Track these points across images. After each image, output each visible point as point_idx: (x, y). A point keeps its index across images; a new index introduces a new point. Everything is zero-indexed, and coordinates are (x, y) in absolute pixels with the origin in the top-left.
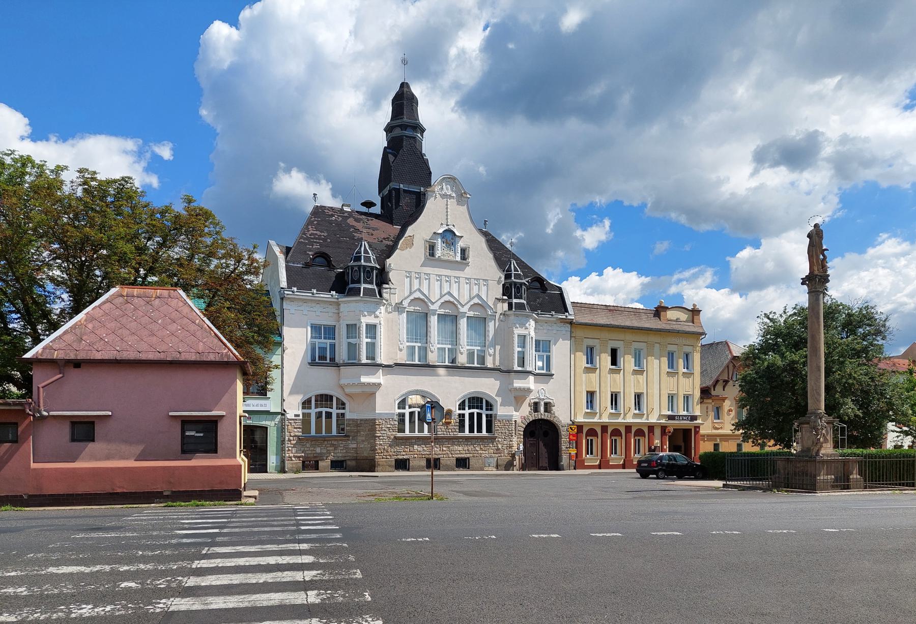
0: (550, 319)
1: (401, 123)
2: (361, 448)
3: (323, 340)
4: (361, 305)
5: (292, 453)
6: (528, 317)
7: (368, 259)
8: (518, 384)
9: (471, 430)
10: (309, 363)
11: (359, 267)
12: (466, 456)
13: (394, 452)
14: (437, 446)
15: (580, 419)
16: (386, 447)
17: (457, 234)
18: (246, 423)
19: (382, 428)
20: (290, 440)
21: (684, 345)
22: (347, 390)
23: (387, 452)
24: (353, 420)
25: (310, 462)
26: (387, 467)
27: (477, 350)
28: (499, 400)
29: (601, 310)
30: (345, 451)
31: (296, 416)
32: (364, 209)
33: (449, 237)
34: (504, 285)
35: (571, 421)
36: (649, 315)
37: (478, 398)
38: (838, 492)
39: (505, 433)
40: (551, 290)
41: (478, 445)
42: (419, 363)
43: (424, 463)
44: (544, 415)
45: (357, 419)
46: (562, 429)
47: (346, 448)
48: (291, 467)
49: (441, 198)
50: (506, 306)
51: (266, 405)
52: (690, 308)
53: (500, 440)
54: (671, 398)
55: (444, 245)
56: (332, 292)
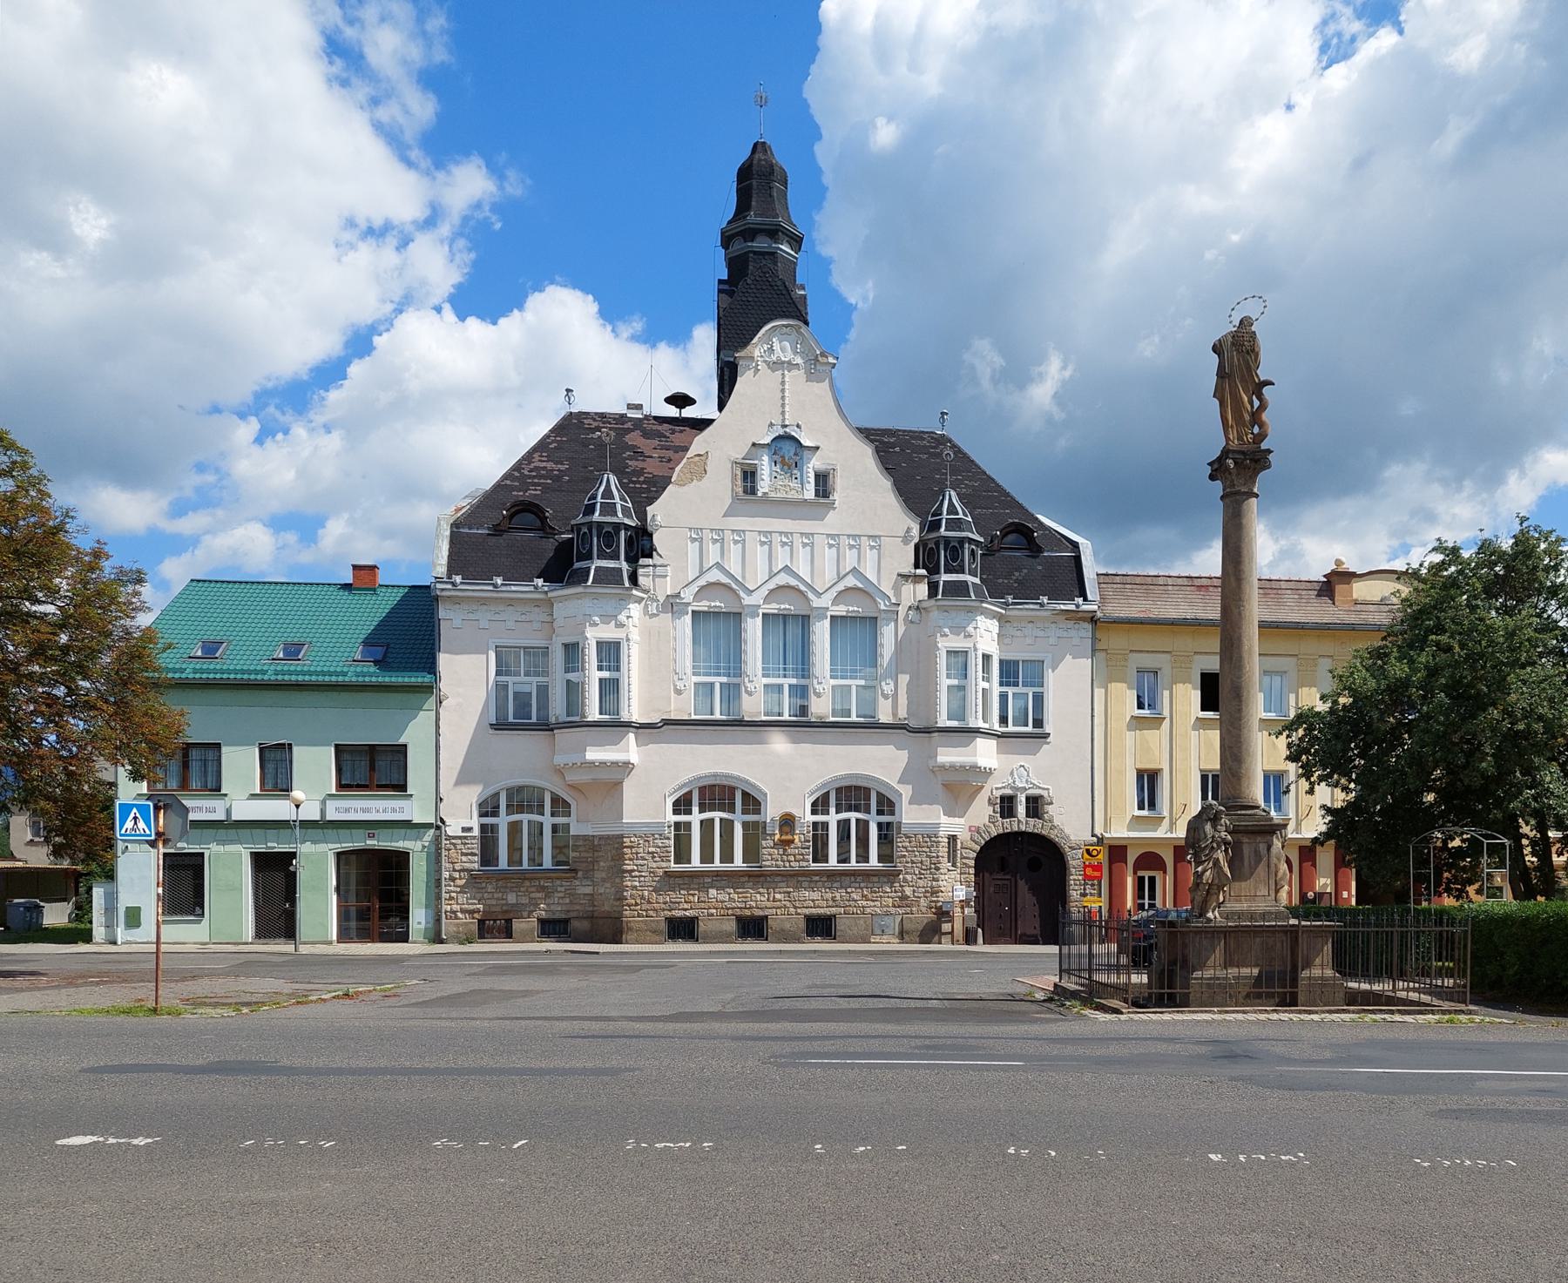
0: (1038, 613)
1: (742, 228)
2: (601, 894)
3: (522, 678)
4: (586, 605)
5: (457, 904)
6: (973, 612)
7: (609, 509)
8: (948, 756)
10: (491, 725)
11: (590, 525)
12: (828, 911)
13: (665, 903)
14: (761, 890)
15: (1119, 831)
16: (646, 893)
17: (806, 442)
18: (366, 845)
20: (453, 879)
22: (572, 778)
23: (649, 902)
24: (585, 838)
25: (495, 921)
27: (721, 684)
28: (906, 791)
29: (1176, 588)
30: (567, 901)
31: (464, 829)
32: (672, 411)
33: (787, 448)
36: (1304, 592)
37: (858, 788)
38: (1202, 1012)
39: (921, 862)
40: (1052, 551)
41: (856, 888)
42: (724, 718)
43: (731, 926)
44: (1027, 823)
46: (1069, 854)
47: (571, 894)
48: (455, 932)
49: (769, 371)
50: (923, 590)
51: (402, 810)
55: (778, 468)
56: (1076, 599)
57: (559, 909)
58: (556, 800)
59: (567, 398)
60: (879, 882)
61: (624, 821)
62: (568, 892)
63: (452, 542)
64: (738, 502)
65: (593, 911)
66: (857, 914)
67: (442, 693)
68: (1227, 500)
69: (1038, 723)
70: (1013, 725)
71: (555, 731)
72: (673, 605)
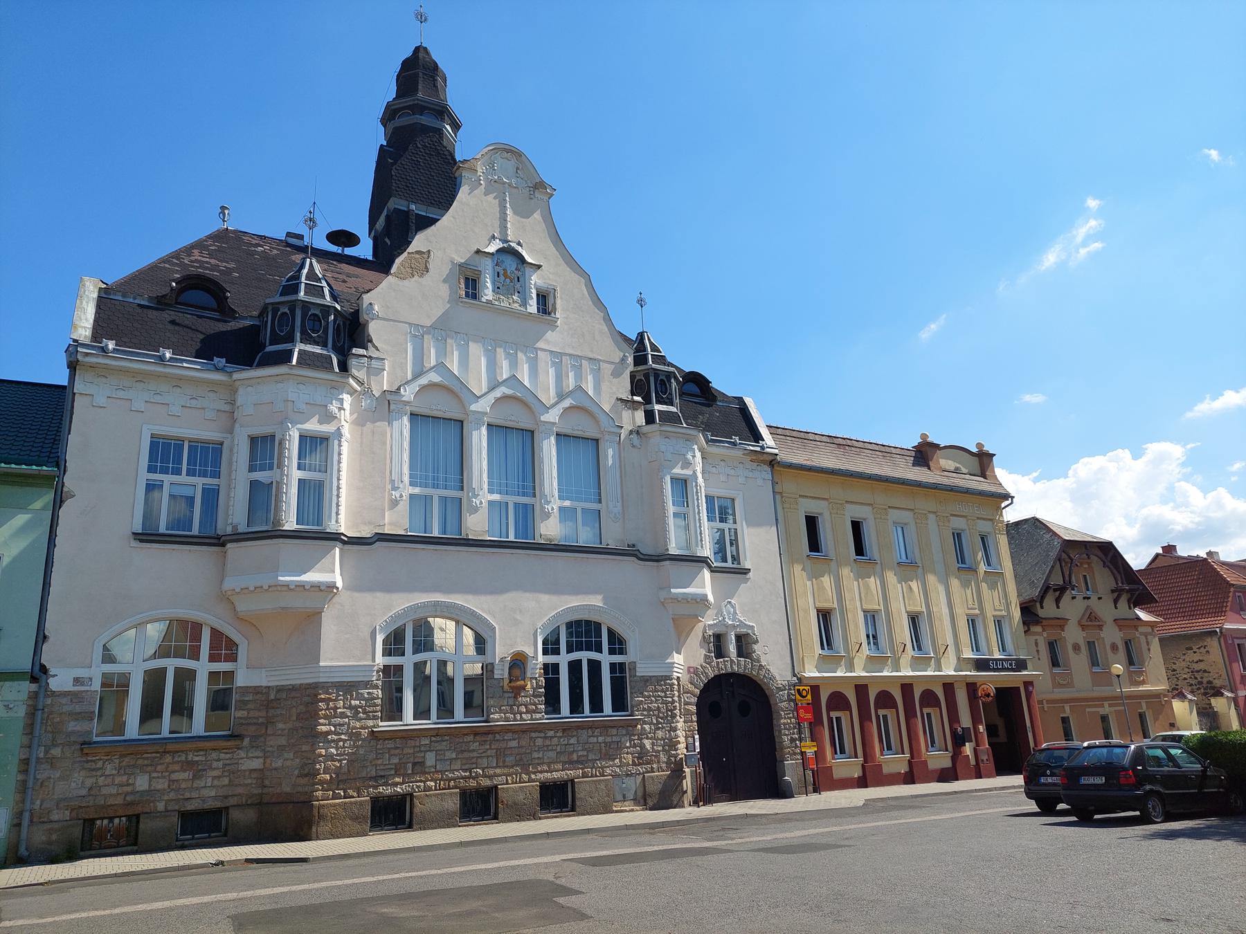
3: (183, 478)
9: (576, 706)
10: (134, 534)
15: (811, 672)
17: (529, 260)
19: (336, 708)
21: (978, 518)
24: (257, 690)
26: (348, 821)
30: (226, 781)
31: (77, 681)
34: (633, 376)
35: (794, 675)
37: (588, 623)
50: (640, 417)
53: (647, 727)
57: (213, 794)
59: (221, 215)
61: (321, 664)
62: (227, 768)
63: (99, 307)
64: (461, 304)
66: (597, 776)
67: (65, 489)
71: (229, 545)
72: (387, 404)
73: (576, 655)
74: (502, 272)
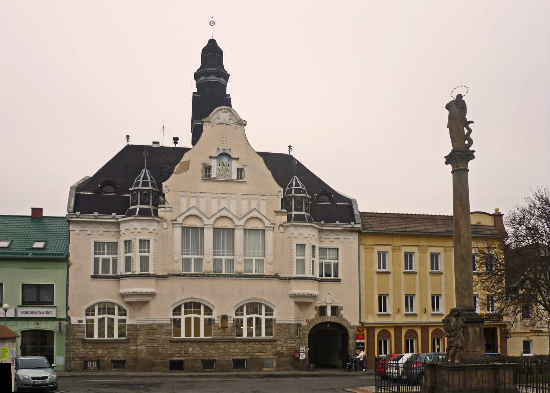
15: (371, 319)
24: (133, 325)
31: (79, 321)
43: (199, 364)
45: (137, 324)
50: (285, 218)
52: (492, 212)
54: (383, 299)
58: (120, 309)
60: (266, 344)
65: (136, 357)
68: (455, 173)
69: (336, 275)
70: (325, 276)
73: (102, 316)
74: (221, 164)
